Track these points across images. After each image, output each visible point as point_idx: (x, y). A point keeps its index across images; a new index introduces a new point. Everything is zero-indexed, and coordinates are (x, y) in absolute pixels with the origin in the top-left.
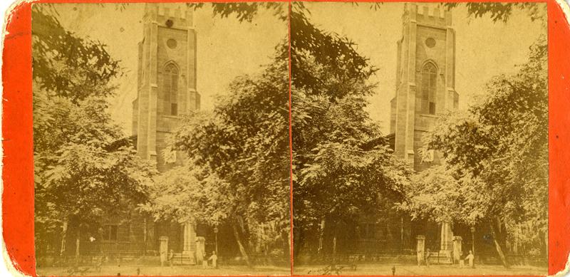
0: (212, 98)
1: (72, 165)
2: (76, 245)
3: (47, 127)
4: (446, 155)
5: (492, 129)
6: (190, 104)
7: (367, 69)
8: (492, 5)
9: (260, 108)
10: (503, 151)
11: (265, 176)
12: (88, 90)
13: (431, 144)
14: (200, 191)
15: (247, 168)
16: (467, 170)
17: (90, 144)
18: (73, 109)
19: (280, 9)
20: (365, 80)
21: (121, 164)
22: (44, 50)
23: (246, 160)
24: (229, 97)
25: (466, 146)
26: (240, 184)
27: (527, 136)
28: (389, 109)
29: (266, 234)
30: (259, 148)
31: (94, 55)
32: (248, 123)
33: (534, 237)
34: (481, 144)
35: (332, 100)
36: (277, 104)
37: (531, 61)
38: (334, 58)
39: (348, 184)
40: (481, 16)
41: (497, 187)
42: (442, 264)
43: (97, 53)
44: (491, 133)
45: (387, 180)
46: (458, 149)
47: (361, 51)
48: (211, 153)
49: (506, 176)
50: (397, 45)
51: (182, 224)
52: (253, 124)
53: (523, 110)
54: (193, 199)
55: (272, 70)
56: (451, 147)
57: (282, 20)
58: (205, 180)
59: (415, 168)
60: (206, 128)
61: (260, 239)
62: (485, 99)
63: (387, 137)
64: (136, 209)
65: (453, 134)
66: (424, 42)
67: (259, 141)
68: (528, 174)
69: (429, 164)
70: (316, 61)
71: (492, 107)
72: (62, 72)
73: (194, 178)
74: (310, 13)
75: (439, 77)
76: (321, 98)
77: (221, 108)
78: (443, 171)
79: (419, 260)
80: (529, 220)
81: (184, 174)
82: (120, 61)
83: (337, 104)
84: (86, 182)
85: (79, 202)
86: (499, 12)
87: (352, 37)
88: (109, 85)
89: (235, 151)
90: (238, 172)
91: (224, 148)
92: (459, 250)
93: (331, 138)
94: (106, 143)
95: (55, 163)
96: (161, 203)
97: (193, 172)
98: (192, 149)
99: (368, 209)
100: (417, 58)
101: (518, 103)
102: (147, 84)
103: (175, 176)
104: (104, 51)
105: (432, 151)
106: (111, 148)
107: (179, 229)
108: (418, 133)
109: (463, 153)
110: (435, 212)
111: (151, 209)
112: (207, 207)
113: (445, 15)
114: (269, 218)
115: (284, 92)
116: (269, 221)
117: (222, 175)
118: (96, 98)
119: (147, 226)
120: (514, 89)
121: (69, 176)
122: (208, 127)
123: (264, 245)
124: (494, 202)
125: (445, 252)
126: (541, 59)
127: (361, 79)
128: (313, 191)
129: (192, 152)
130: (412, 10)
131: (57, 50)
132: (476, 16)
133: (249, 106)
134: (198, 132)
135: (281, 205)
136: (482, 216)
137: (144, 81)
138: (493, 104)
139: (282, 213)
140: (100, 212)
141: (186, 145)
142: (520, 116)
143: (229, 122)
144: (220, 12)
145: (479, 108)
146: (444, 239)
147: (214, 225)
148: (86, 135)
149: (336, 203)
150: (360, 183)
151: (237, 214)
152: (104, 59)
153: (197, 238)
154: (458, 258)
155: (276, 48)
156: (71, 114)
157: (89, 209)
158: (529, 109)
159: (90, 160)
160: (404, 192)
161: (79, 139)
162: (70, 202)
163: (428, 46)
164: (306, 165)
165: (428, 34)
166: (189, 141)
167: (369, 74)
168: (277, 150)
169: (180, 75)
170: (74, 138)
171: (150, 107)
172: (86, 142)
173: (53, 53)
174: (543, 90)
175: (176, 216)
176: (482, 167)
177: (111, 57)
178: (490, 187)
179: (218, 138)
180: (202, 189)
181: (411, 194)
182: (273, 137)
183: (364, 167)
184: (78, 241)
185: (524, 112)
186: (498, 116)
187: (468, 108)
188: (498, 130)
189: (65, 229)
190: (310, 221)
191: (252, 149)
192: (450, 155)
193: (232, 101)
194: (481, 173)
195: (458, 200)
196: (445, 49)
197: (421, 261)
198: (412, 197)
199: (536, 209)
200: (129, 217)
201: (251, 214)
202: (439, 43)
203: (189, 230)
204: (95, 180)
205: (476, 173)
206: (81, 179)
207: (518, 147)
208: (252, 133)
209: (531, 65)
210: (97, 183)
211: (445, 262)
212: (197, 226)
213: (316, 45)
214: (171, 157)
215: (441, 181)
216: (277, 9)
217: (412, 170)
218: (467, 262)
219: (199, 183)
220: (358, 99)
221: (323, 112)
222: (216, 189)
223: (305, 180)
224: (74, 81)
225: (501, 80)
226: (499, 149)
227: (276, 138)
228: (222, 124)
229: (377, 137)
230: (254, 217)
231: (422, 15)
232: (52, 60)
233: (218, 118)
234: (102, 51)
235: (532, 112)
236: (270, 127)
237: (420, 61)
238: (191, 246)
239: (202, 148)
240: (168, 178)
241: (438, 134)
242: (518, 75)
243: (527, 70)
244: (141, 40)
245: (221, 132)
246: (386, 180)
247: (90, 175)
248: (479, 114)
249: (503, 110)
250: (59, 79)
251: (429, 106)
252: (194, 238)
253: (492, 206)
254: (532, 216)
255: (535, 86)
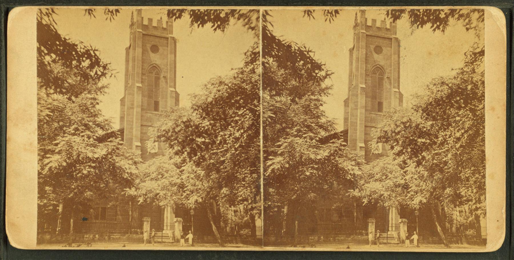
0: (190, 96)
1: (290, 156)
2: (70, 224)
3: (45, 121)
4: (392, 148)
5: (432, 125)
6: (170, 102)
7: (323, 73)
8: (431, 17)
9: (231, 106)
10: (442, 144)
11: (235, 165)
12: (81, 89)
13: (379, 138)
14: (178, 178)
15: (220, 158)
16: (411, 161)
17: (83, 136)
18: (69, 105)
19: (249, 20)
20: (322, 83)
21: (110, 153)
22: (43, 54)
23: (219, 151)
24: (426, 96)
25: (410, 140)
26: (213, 172)
27: (463, 131)
28: (342, 108)
29: (235, 216)
30: (230, 141)
31: (87, 58)
32: (221, 119)
33: (470, 219)
34: (423, 138)
35: (293, 101)
36: (246, 103)
37: (466, 66)
38: (294, 64)
39: (308, 174)
40: (422, 27)
41: (438, 176)
42: (390, 243)
43: (90, 57)
44: (432, 128)
45: (119, 169)
46: (404, 142)
47: (317, 57)
48: (188, 145)
49: (446, 165)
50: (349, 52)
51: (163, 207)
52: (225, 120)
53: (459, 108)
54: (173, 185)
55: (242, 73)
56: (397, 141)
57: (250, 30)
58: (183, 168)
59: (366, 159)
60: (184, 123)
61: (230, 221)
62: (426, 98)
63: (341, 132)
64: (123, 193)
65: (399, 129)
66: (372, 49)
67: (230, 135)
68: (464, 164)
69: (379, 156)
70: (278, 66)
71: (432, 105)
72: (58, 72)
73: (173, 166)
74: (272, 25)
75: (162, 79)
76: (283, 99)
77: (197, 106)
78: (390, 162)
79: (370, 240)
80: (466, 204)
81: (165, 163)
82: (325, 65)
83: (297, 104)
84: (79, 169)
85: (73, 187)
86: (438, 23)
87: (309, 46)
88: (100, 85)
89: (209, 143)
90: (212, 161)
91: (200, 140)
92: (405, 231)
93: (292, 133)
94: (97, 135)
95: (53, 152)
96: (145, 188)
97: (172, 161)
98: (171, 141)
99: (103, 194)
100: (142, 63)
101: (455, 102)
102: (133, 84)
103: (381, 164)
104: (95, 55)
105: (380, 145)
106: (101, 140)
107: (160, 211)
108: (145, 128)
109: (407, 145)
110: (384, 198)
111: (135, 193)
112: (184, 192)
113: (391, 26)
114: (238, 202)
115: (252, 92)
116: (238, 205)
117: (198, 164)
118: (89, 96)
119: (132, 208)
120: (452, 90)
121: (64, 164)
122: (186, 122)
123: (233, 226)
124: (211, 188)
125: (168, 232)
126: (475, 64)
127: (317, 82)
128: (278, 180)
129: (172, 143)
130: (361, 22)
131: (55, 54)
132: (418, 28)
133: (221, 105)
134: (177, 126)
135: (249, 191)
136: (425, 201)
137: (130, 82)
138: (433, 103)
139: (249, 198)
140: (92, 196)
141: (166, 137)
142: (457, 113)
143: (204, 118)
144: (197, 22)
145: (421, 107)
146: (392, 222)
147: (415, 208)
148: (80, 128)
149: (297, 191)
150: (318, 173)
151: (211, 198)
152: (96, 62)
153: (175, 219)
154: (179, 237)
155: (245, 54)
156: (68, 110)
157: (82, 193)
158: (464, 108)
159: (83, 151)
160: (357, 181)
161: (74, 131)
162: (65, 186)
163: (153, 52)
164: (271, 157)
165: (151, 42)
166: (170, 134)
167: (325, 78)
168: (245, 143)
169: (385, 77)
170: (69, 130)
171: (135, 104)
172: (79, 134)
173: (51, 57)
174: (477, 91)
175: (158, 200)
176: (424, 158)
177: (102, 60)
178: (431, 176)
179: (195, 132)
180: (180, 176)
181: (362, 182)
182: (242, 131)
183: (321, 159)
184: (72, 220)
185: (460, 110)
186: (437, 113)
187: (411, 106)
188: (438, 126)
189: (60, 210)
190: (275, 207)
191: (224, 141)
192: (396, 148)
193: (207, 99)
194: (424, 163)
195: (179, 186)
196: (391, 55)
197: (147, 239)
198: (363, 185)
199: (472, 195)
200: (116, 199)
201: (222, 198)
202: (385, 50)
203: (394, 214)
204: (87, 167)
205: (419, 163)
206: (75, 167)
207: (455, 140)
208: (224, 128)
209: (466, 69)
210: (89, 170)
211: (393, 242)
212: (176, 209)
213: (278, 53)
214: (153, 148)
215: (165, 169)
216: (246, 20)
217: (363, 161)
218: (187, 240)
219: (178, 171)
220: (315, 100)
221: (285, 111)
222: (192, 176)
223: (270, 170)
224: (70, 81)
225: (440, 82)
226: (439, 142)
227: (245, 132)
228: (198, 120)
229: (332, 133)
230: (225, 201)
231: (371, 27)
232: (50, 62)
233: (194, 114)
234: (93, 55)
235: (467, 110)
236: (240, 122)
237: (369, 66)
238: (395, 227)
239: (180, 140)
240: (150, 167)
241: (385, 129)
242: (455, 78)
243: (462, 73)
244: (128, 45)
245: (197, 127)
246: (341, 169)
247: (83, 163)
248: (421, 112)
249: (441, 108)
250: (56, 79)
251: (377, 105)
252: (173, 220)
253: (433, 192)
254: (468, 201)
255: (469, 87)
